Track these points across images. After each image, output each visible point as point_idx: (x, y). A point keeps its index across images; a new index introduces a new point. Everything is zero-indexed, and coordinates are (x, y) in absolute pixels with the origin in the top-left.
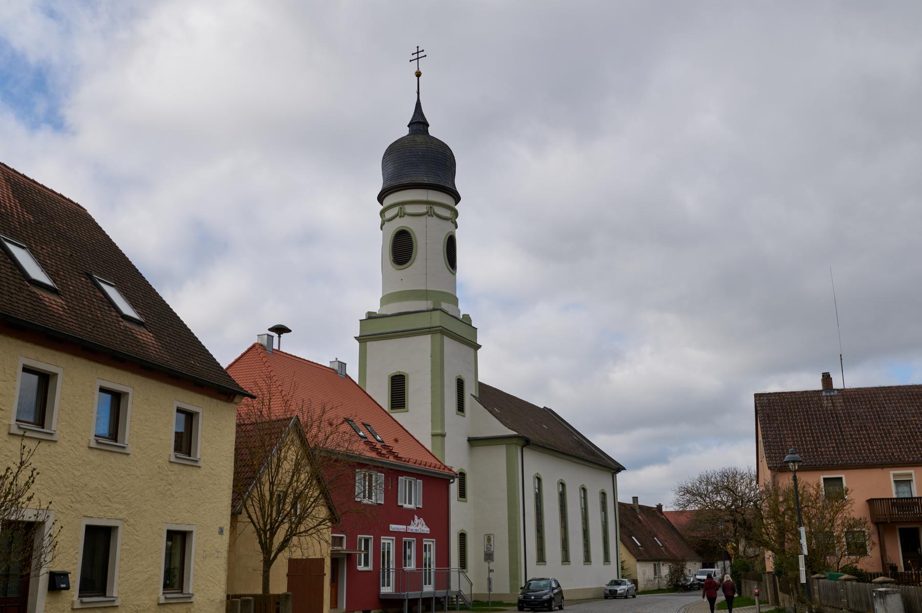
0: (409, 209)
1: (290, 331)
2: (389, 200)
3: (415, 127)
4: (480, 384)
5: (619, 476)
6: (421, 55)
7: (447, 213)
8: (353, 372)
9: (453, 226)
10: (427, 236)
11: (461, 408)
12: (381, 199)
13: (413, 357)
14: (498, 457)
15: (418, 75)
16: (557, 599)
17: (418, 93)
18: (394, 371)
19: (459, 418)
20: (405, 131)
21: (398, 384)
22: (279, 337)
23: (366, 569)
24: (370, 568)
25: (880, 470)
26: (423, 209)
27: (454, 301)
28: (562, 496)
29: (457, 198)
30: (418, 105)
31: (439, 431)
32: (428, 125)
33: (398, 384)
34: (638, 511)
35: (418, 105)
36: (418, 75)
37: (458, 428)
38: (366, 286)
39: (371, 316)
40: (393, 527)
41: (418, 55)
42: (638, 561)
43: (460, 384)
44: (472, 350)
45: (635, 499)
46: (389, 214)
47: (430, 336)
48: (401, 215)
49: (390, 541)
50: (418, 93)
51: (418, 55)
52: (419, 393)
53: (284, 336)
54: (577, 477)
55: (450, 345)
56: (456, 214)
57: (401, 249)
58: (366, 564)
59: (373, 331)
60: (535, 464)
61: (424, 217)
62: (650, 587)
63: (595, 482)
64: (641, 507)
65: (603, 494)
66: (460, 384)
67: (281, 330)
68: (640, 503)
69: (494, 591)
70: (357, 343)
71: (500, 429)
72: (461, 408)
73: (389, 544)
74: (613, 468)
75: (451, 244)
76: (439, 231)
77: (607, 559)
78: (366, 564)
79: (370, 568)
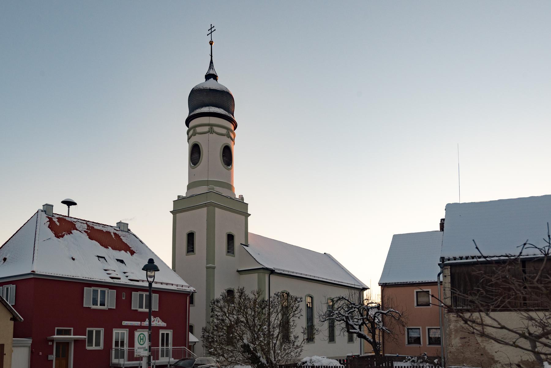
1: (63, 202)
2: (192, 124)
6: (213, 29)
12: (187, 122)
15: (211, 43)
16: (493, 361)
17: (211, 56)
18: (188, 231)
22: (69, 207)
23: (97, 348)
24: (101, 347)
25: (118, 251)
26: (206, 129)
27: (230, 187)
30: (211, 62)
36: (211, 43)
40: (125, 323)
41: (212, 30)
44: (243, 217)
47: (206, 208)
49: (125, 332)
50: (211, 56)
51: (212, 30)
53: (72, 207)
58: (98, 344)
70: (172, 215)
73: (167, 334)
78: (98, 344)
79: (101, 347)
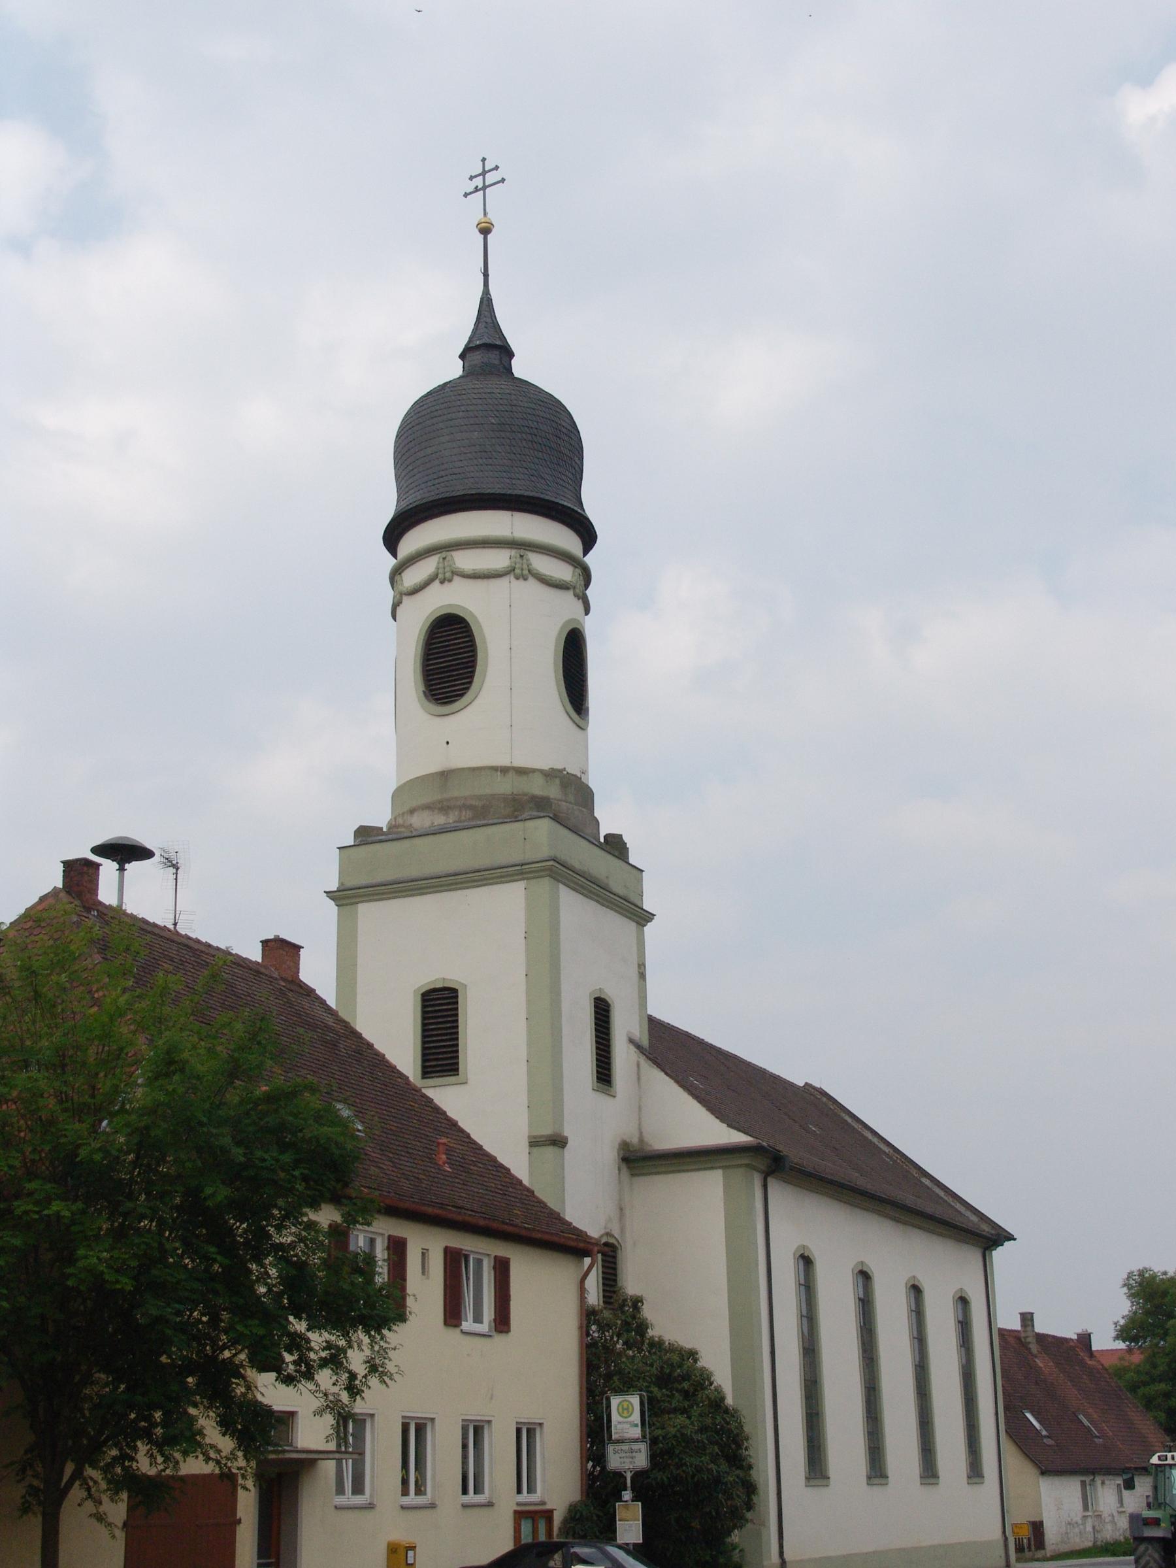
0: (466, 560)
3: (477, 358)
4: (652, 1020)
5: (999, 1255)
6: (491, 178)
7: (564, 572)
8: (318, 972)
9: (579, 605)
10: (514, 630)
11: (604, 1074)
12: (392, 537)
13: (479, 940)
14: (705, 1197)
15: (485, 231)
17: (486, 275)
19: (602, 1099)
20: (454, 369)
21: (440, 1011)
22: (122, 869)
26: (499, 559)
28: (866, 1305)
29: (588, 537)
30: (486, 305)
31: (547, 1131)
32: (511, 355)
33: (440, 1011)
34: (1034, 1348)
35: (486, 305)
36: (485, 231)
37: (597, 1125)
38: (358, 743)
39: (365, 835)
41: (483, 181)
42: (1043, 1473)
43: (602, 1011)
45: (1027, 1319)
46: (412, 577)
48: (443, 577)
50: (486, 275)
51: (483, 181)
52: (492, 1035)
54: (900, 1257)
55: (573, 907)
56: (586, 576)
57: (448, 661)
59: (376, 870)
60: (800, 1223)
61: (503, 582)
62: (1065, 1548)
63: (945, 1270)
64: (1042, 1338)
65: (963, 1301)
66: (602, 1011)
67: (125, 852)
68: (1040, 1328)
69: (1078, 1484)
70: (331, 907)
71: (707, 1129)
72: (604, 1074)
74: (987, 1238)
75: (573, 652)
76: (549, 614)
77: (975, 1471)
